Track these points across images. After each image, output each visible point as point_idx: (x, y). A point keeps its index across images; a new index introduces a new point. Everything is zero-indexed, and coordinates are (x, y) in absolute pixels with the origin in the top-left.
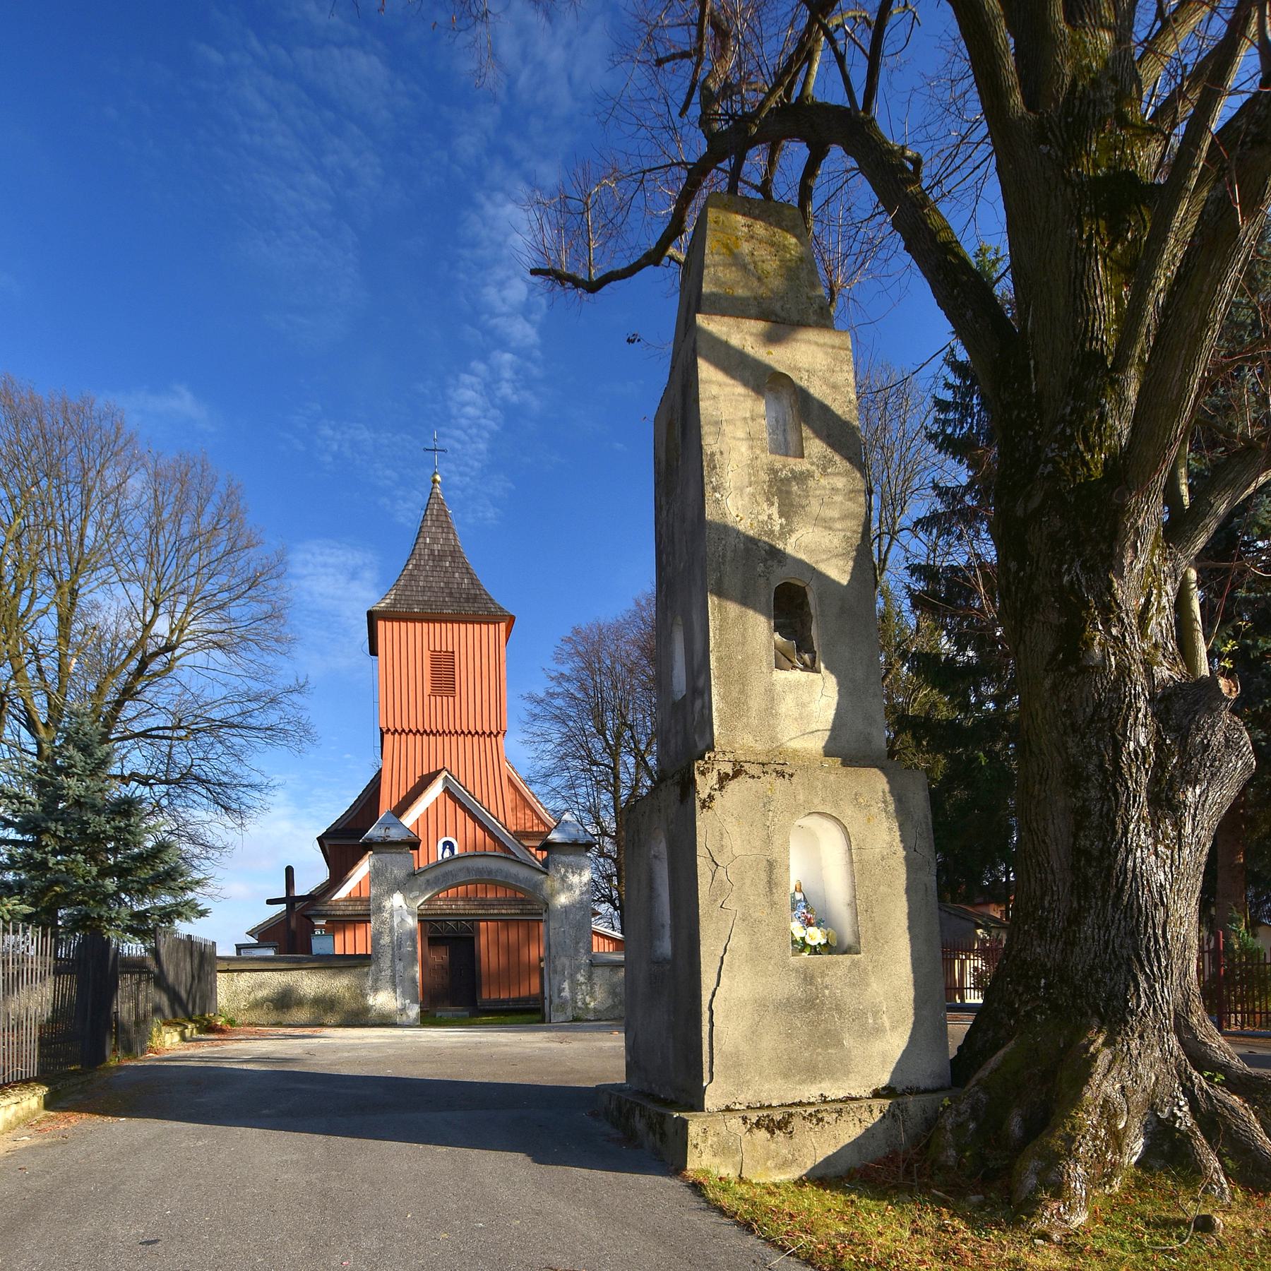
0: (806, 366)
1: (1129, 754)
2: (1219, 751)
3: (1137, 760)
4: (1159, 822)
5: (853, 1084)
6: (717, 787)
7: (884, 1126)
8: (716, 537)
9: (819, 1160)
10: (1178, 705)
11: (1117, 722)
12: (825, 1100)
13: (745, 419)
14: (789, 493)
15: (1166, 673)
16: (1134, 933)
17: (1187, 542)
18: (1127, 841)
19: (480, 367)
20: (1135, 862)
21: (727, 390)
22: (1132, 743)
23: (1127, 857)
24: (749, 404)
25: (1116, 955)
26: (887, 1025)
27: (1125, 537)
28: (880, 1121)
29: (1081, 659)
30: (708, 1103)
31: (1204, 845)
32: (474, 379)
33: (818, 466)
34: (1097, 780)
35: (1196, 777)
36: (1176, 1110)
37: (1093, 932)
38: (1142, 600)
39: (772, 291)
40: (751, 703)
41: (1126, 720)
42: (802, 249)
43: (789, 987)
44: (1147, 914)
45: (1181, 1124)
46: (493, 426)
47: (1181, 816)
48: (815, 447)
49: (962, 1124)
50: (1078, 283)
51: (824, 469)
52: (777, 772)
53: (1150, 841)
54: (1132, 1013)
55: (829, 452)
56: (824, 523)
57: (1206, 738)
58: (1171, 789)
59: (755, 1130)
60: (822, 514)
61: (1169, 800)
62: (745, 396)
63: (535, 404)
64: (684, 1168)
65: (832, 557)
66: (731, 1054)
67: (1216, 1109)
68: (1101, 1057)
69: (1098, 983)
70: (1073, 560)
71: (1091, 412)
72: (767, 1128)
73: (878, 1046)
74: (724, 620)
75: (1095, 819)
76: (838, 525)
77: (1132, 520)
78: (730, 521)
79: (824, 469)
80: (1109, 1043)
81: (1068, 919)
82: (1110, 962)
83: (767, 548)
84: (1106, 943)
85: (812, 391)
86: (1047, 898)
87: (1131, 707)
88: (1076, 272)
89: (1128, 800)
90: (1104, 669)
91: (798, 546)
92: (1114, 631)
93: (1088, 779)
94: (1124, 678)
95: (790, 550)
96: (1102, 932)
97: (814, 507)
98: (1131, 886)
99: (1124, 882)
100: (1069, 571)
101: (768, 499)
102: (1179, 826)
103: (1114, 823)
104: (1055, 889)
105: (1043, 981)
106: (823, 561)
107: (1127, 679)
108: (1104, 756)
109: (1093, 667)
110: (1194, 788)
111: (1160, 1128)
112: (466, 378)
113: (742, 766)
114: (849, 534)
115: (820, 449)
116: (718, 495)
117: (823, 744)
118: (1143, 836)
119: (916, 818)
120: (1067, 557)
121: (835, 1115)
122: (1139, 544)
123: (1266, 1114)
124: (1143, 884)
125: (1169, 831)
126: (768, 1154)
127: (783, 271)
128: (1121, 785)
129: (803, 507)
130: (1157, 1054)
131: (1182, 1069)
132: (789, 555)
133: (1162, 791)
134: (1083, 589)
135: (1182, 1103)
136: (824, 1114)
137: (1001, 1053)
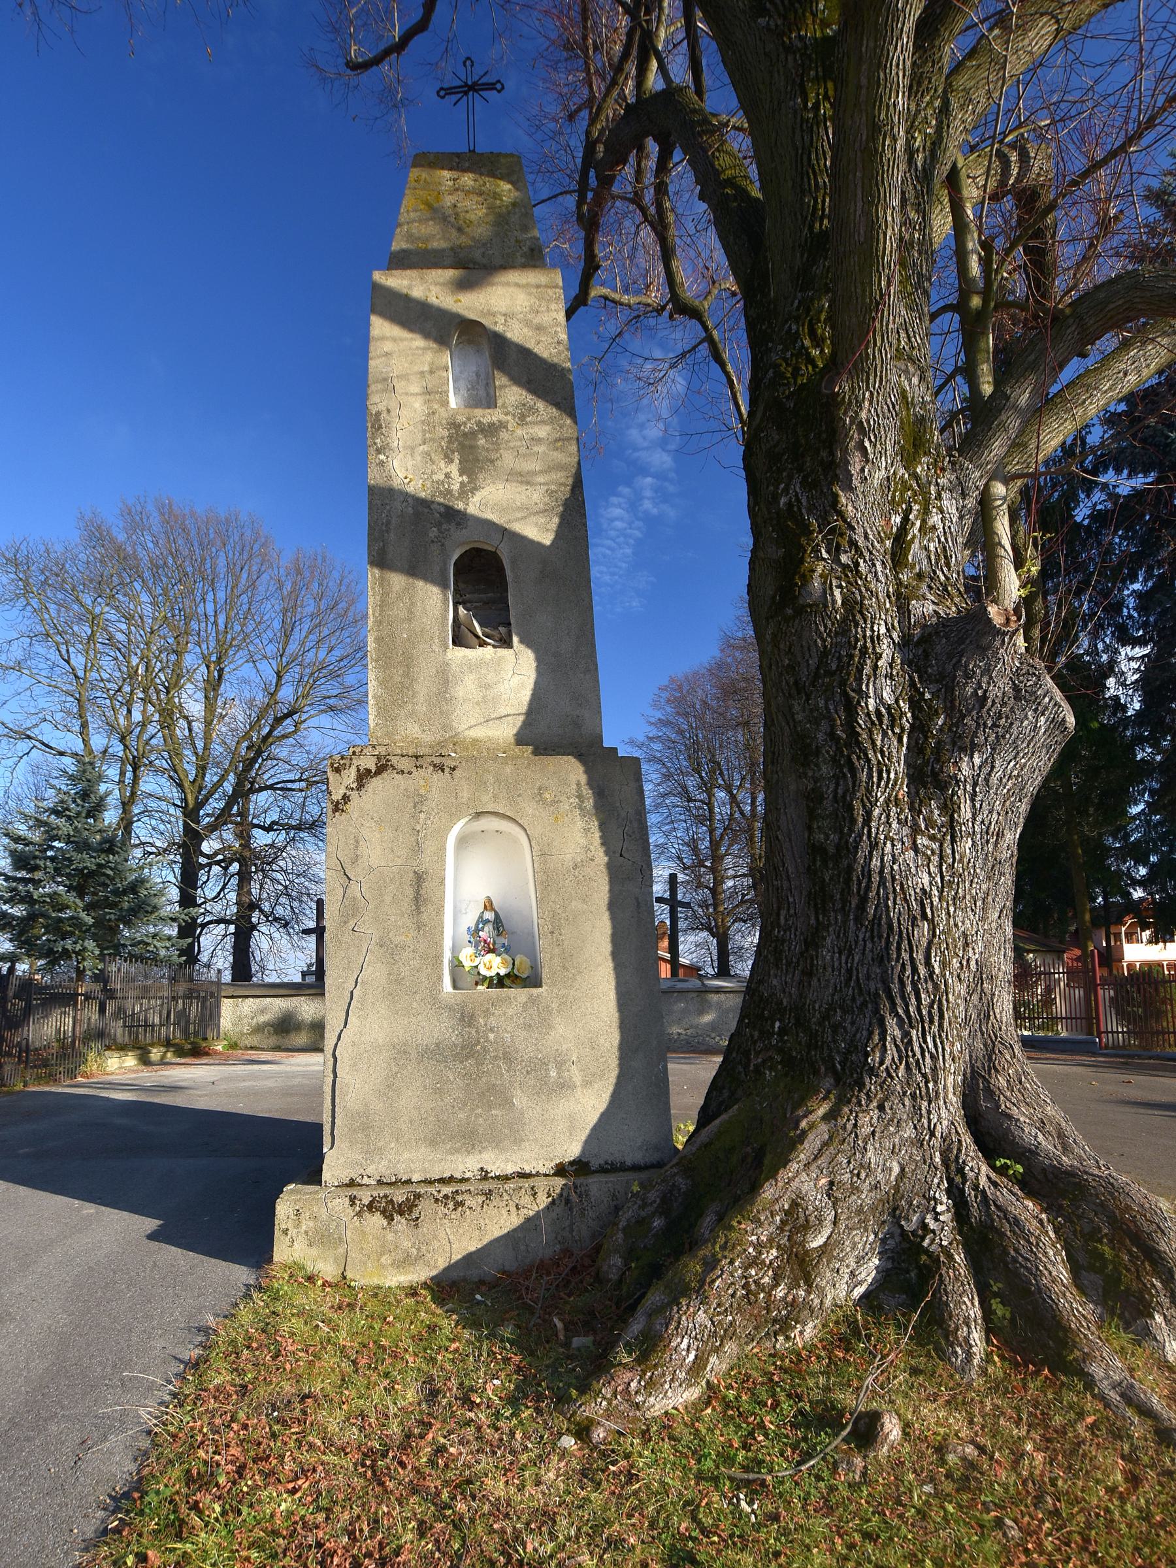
0: (503, 310)
1: (868, 715)
2: (1004, 704)
3: (881, 723)
4: (920, 805)
5: (526, 1156)
6: (354, 786)
7: (554, 1215)
8: (379, 502)
9: (457, 1257)
10: (940, 646)
11: (849, 674)
12: (485, 1176)
13: (422, 372)
14: (473, 447)
15: (929, 608)
16: (882, 959)
17: (979, 447)
18: (870, 832)
19: (626, 490)
20: (882, 860)
21: (403, 345)
22: (871, 701)
23: (871, 853)
24: (429, 356)
25: (860, 989)
26: (577, 1079)
27: (846, 436)
28: (547, 1208)
29: (796, 598)
30: (326, 1175)
31: (1000, 835)
32: (621, 500)
33: (514, 415)
34: (828, 752)
35: (972, 741)
36: (929, 1219)
37: (832, 958)
38: (897, 520)
39: (473, 238)
40: (418, 687)
41: (860, 671)
42: (517, 194)
43: (442, 1030)
44: (901, 932)
45: (933, 1241)
46: (638, 534)
47: (953, 795)
48: (512, 395)
49: (644, 1219)
50: (805, 158)
51: (523, 417)
52: (435, 766)
53: (906, 831)
54: (872, 1071)
55: (530, 398)
56: (524, 478)
57: (980, 687)
58: (938, 760)
59: (367, 1215)
60: (518, 468)
61: (935, 775)
62: (424, 349)
63: (671, 513)
64: (270, 1260)
65: (530, 514)
66: (358, 1114)
67: (993, 1221)
68: (811, 1136)
69: (835, 1028)
70: (790, 477)
71: (820, 299)
72: (384, 1213)
73: (562, 1107)
74: (385, 595)
75: (828, 804)
76: (541, 479)
77: (851, 413)
78: (396, 483)
79: (523, 417)
80: (831, 1116)
81: (805, 941)
82: (853, 1000)
83: (442, 510)
84: (849, 971)
85: (509, 335)
86: (783, 913)
87: (866, 653)
88: (803, 149)
89: (870, 776)
90: (826, 606)
91: (484, 504)
92: (844, 559)
93: (817, 752)
94: (854, 616)
95: (472, 510)
96: (843, 958)
97: (508, 460)
98: (878, 893)
99: (868, 888)
100: (786, 490)
101: (446, 456)
102: (949, 808)
103: (851, 808)
104: (791, 900)
105: (777, 1024)
106: (518, 520)
107: (858, 617)
108: (835, 720)
109: (810, 606)
110: (972, 757)
111: (905, 1245)
112: (614, 500)
113: (388, 760)
114: (553, 487)
115: (517, 397)
116: (382, 457)
117: (515, 731)
118: (895, 825)
119: (623, 814)
120: (785, 474)
121: (481, 1199)
122: (867, 444)
123: (1075, 1232)
124: (895, 889)
125: (936, 817)
126: (383, 1246)
127: (491, 218)
128: (859, 758)
129: (492, 462)
130: (908, 1132)
131: (953, 1157)
132: (472, 516)
133: (926, 763)
134: (804, 511)
135: (939, 1209)
136: (466, 1196)
137: (717, 1122)
